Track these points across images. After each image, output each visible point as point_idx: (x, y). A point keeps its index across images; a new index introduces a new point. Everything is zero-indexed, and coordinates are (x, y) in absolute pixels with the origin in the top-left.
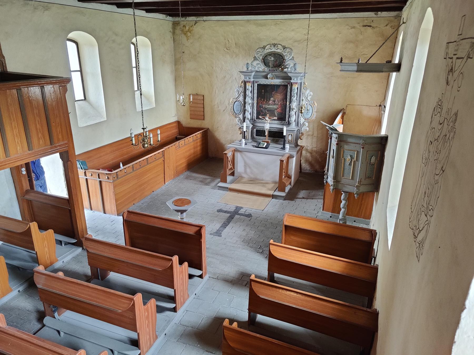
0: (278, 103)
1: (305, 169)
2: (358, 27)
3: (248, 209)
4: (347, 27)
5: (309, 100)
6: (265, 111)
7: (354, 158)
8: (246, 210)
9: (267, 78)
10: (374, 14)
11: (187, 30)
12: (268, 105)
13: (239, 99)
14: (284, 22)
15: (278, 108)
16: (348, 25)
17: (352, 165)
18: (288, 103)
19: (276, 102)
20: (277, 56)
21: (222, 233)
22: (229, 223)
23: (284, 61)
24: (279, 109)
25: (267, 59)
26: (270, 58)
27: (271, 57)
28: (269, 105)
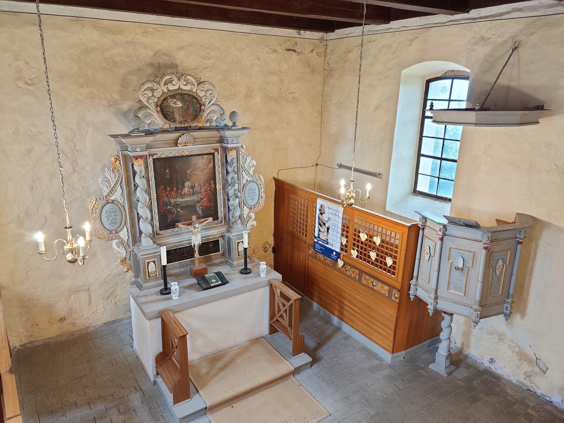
0: (201, 189)
2: (281, 51)
4: (267, 49)
5: (252, 175)
6: (177, 210)
10: (297, 33)
12: (181, 198)
13: (112, 198)
14: (163, 30)
15: (201, 198)
16: (267, 46)
19: (197, 189)
20: (187, 98)
23: (203, 108)
24: (204, 200)
26: (175, 103)
27: (175, 100)
28: (183, 196)
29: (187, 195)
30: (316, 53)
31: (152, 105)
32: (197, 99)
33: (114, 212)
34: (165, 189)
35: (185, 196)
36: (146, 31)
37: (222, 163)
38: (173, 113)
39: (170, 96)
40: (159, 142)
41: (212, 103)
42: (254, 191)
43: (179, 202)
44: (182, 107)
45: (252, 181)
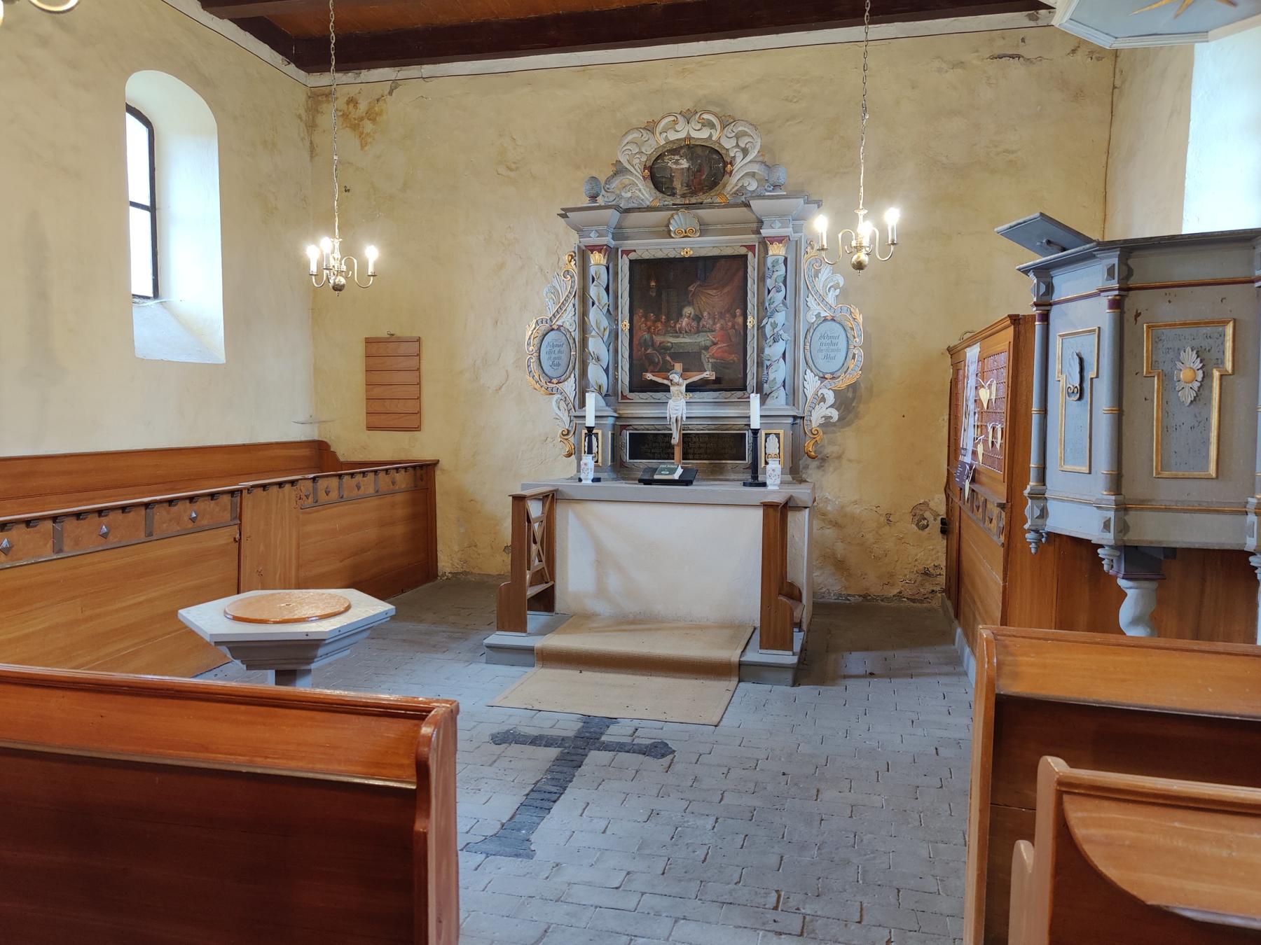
0: (714, 324)
1: (824, 590)
2: (975, 62)
3: (644, 723)
5: (833, 306)
7: (1219, 363)
8: (633, 729)
9: (668, 234)
11: (364, 114)
13: (559, 323)
14: (712, 62)
15: (712, 342)
17: (1210, 399)
18: (751, 321)
19: (707, 321)
21: (533, 838)
22: (565, 790)
25: (666, 168)
26: (677, 163)
27: (677, 157)
29: (686, 332)
30: (1087, 53)
31: (636, 167)
32: (720, 154)
33: (559, 346)
34: (646, 316)
35: (681, 333)
36: (683, 69)
37: (760, 276)
38: (671, 179)
39: (667, 151)
40: (642, 230)
41: (749, 160)
42: (834, 341)
43: (669, 344)
44: (689, 169)
45: (829, 318)
